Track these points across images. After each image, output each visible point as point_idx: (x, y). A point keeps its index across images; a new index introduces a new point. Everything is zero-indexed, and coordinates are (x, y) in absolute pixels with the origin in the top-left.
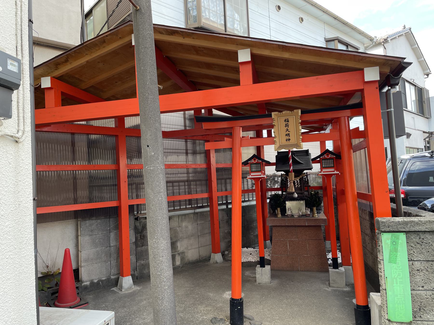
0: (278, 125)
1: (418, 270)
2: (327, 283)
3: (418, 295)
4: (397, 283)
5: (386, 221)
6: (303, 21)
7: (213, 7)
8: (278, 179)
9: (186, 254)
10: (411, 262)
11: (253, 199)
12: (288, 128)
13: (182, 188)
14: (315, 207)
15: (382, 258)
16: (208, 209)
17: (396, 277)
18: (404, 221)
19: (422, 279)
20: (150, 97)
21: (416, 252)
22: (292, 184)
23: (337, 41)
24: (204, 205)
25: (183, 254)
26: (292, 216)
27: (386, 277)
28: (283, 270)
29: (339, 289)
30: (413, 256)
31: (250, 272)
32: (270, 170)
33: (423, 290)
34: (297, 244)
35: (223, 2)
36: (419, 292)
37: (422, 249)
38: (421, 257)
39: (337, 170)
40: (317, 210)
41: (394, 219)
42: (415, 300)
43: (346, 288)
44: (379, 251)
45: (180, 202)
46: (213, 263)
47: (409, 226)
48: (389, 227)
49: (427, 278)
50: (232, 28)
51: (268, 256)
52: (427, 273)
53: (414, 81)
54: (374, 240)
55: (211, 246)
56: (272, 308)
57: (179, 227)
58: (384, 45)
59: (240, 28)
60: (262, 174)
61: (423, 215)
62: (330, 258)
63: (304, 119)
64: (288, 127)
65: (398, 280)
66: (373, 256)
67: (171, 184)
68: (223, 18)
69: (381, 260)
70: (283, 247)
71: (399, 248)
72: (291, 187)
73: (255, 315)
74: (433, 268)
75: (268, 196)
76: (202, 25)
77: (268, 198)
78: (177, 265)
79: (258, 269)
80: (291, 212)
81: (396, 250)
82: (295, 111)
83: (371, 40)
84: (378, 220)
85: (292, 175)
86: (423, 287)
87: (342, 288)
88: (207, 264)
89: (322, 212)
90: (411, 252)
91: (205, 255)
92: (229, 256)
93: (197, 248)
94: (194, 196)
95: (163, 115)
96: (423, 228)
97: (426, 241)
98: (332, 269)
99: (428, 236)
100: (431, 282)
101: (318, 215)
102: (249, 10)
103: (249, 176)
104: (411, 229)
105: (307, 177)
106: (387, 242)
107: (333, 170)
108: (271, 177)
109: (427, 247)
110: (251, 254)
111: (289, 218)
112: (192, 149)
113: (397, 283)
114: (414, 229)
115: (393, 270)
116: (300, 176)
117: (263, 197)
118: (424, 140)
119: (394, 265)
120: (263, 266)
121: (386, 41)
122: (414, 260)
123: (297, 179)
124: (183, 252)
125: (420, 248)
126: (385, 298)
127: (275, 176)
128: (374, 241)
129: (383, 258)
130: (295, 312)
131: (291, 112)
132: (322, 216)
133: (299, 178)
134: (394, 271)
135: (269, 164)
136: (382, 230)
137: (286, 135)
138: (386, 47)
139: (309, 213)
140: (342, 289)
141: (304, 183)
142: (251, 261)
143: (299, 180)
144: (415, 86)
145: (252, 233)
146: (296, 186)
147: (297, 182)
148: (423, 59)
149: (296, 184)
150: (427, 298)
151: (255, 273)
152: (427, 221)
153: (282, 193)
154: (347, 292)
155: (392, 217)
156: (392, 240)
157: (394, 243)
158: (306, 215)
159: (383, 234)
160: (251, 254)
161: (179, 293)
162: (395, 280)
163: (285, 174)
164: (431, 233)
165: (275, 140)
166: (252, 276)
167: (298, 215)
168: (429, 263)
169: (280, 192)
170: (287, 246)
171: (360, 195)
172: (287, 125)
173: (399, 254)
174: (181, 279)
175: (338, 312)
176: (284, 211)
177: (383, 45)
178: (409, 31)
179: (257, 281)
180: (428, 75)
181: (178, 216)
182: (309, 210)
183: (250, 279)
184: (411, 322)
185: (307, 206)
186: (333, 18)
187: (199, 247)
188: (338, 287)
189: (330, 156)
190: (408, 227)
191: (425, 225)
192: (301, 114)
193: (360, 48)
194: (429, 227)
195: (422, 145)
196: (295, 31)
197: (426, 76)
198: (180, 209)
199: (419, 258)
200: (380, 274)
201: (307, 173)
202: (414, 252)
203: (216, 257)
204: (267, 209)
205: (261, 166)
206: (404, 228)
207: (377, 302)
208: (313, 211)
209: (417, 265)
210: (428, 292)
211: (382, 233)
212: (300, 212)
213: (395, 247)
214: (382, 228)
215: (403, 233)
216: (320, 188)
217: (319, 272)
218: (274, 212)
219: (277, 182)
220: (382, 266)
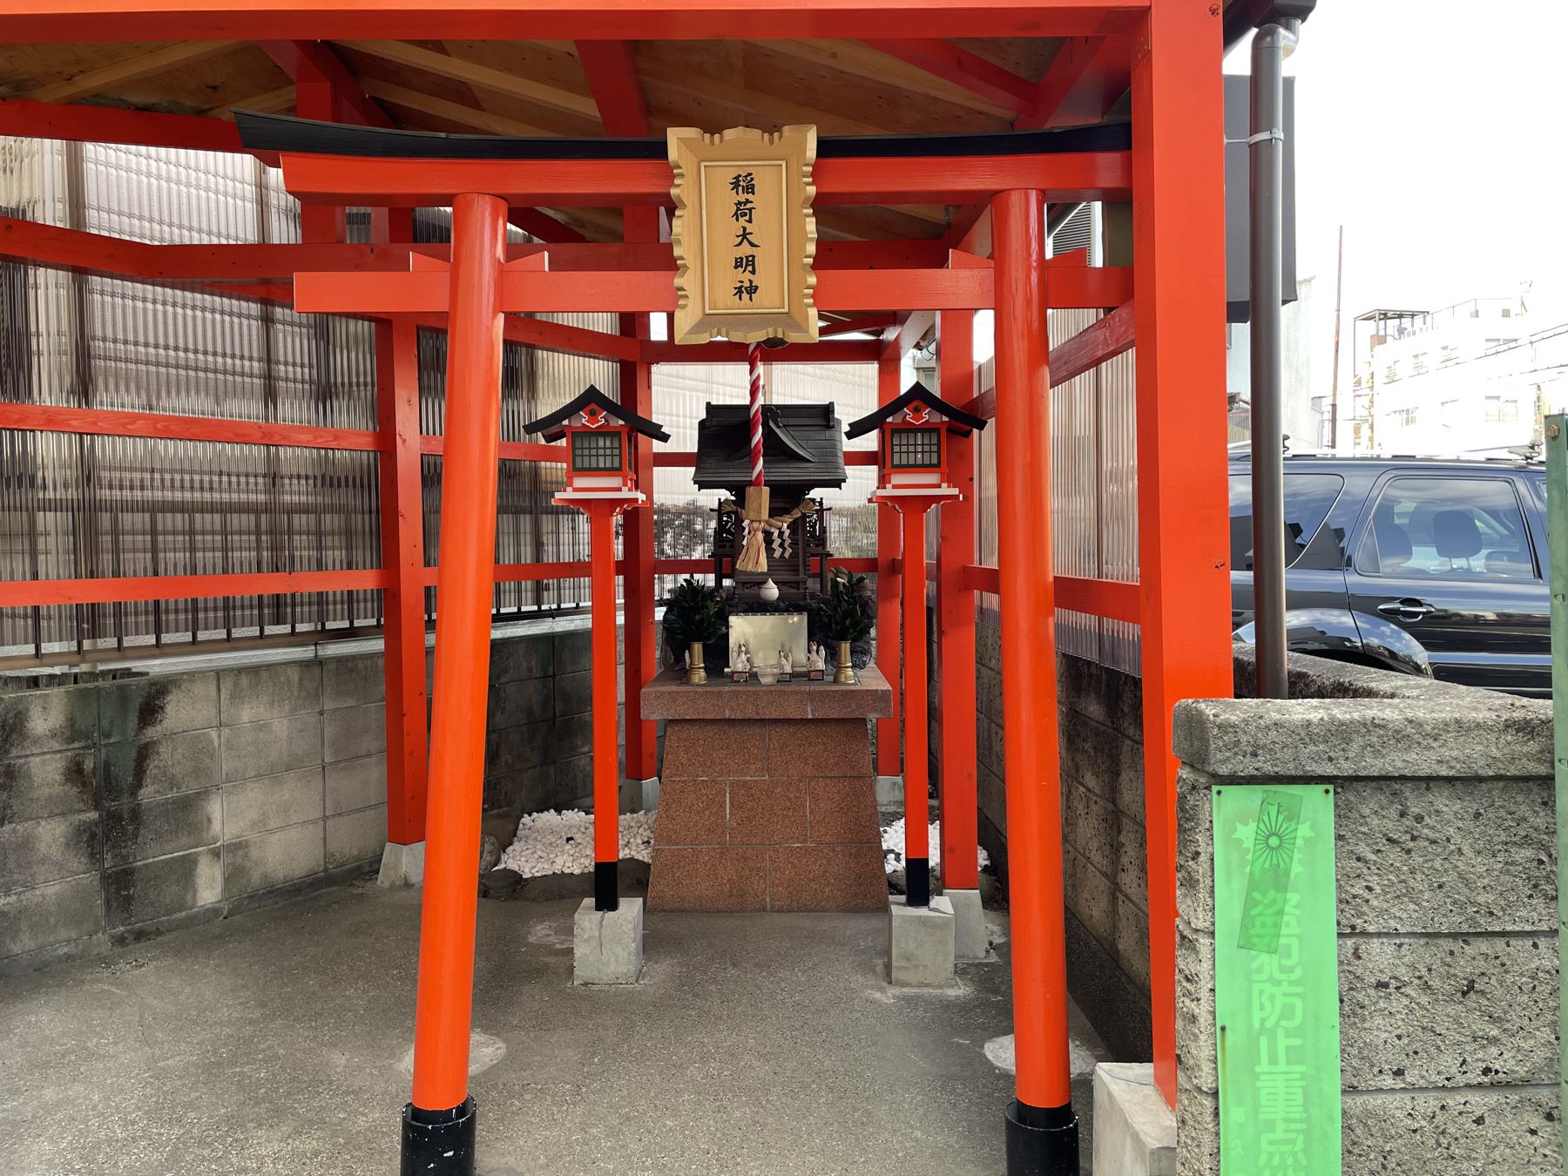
0: (697, 204)
1: (1381, 985)
3: (1369, 1114)
4: (1273, 1060)
5: (1244, 720)
8: (705, 526)
9: (254, 853)
10: (1350, 942)
12: (747, 225)
13: (236, 545)
14: (845, 639)
15: (1207, 924)
16: (378, 645)
17: (1268, 1025)
18: (1333, 720)
19: (1399, 1032)
21: (1378, 889)
22: (760, 536)
24: (357, 623)
25: (241, 853)
26: (753, 676)
27: (1223, 1029)
28: (702, 911)
29: (925, 991)
30: (1365, 908)
31: (554, 925)
33: (1397, 1087)
37: (1413, 872)
39: (952, 483)
40: (852, 652)
41: (1279, 711)
42: (1355, 1143)
43: (957, 985)
44: (1191, 883)
45: (195, 610)
46: (392, 885)
47: (1354, 749)
48: (1256, 755)
49: (1423, 1028)
51: (643, 847)
52: (1424, 1000)
54: (1082, 785)
55: (385, 809)
56: (628, 1119)
60: (625, 484)
61: (1385, 687)
62: (892, 847)
63: (827, 189)
64: (750, 221)
65: (1282, 1042)
66: (1071, 849)
69: (1197, 931)
70: (707, 812)
71: (1296, 868)
72: (755, 549)
73: (541, 1167)
74: (1452, 971)
75: (661, 594)
77: (662, 603)
78: (200, 903)
79: (587, 917)
80: (748, 660)
81: (1279, 880)
84: (1200, 713)
85: (760, 497)
86: (1399, 1073)
87: (941, 987)
88: (360, 891)
89: (872, 664)
90: (1353, 891)
91: (355, 852)
93: (315, 822)
94: (306, 583)
95: (228, 237)
96: (1421, 762)
97: (1433, 828)
98: (904, 905)
99: (1444, 803)
100: (1438, 1048)
101: (855, 675)
103: (565, 491)
104: (1365, 768)
105: (821, 518)
106: (1236, 835)
107: (933, 478)
108: (679, 515)
109: (1437, 864)
110: (571, 839)
111: (740, 689)
112: (306, 361)
113: (1273, 1060)
114: (1379, 763)
115: (1256, 988)
116: (796, 510)
117: (638, 601)
119: (1264, 957)
120: (607, 902)
122: (1364, 934)
123: (780, 524)
124: (240, 843)
125: (1398, 869)
126: (1207, 1139)
127: (693, 511)
128: (1081, 788)
129: (1213, 924)
130: (737, 1133)
131: (766, 136)
132: (871, 679)
133: (788, 519)
134: (1261, 992)
136: (1221, 772)
137: (738, 263)
139: (821, 665)
140: (938, 992)
142: (567, 871)
143: (788, 527)
145: (586, 749)
146: (777, 554)
147: (781, 534)
149: (775, 545)
150: (1415, 1131)
151: (570, 932)
152: (1446, 725)
153: (719, 581)
154: (962, 1007)
155: (1237, 696)
156: (1262, 826)
157: (1274, 841)
158: (807, 676)
159: (1219, 793)
160: (571, 839)
161: (170, 1062)
162: (1263, 1041)
163: (733, 498)
164: (1458, 785)
166: (558, 946)
167: (774, 675)
168: (1436, 945)
169: (709, 580)
170: (722, 806)
171: (1071, 593)
172: (743, 211)
173: (1293, 897)
174: (206, 976)
175: (925, 1114)
176: (718, 654)
179: (577, 972)
181: (218, 673)
182: (823, 652)
183: (547, 965)
187: (325, 818)
188: (922, 985)
189: (927, 415)
190: (1351, 755)
191: (1435, 744)
194: (1455, 753)
198: (230, 643)
199: (1393, 923)
200: (1184, 1004)
202: (1370, 889)
203: (404, 859)
204: (655, 652)
205: (620, 448)
206: (1330, 759)
207: (1137, 1127)
208: (840, 658)
209: (1380, 957)
210: (1420, 1098)
211: (1215, 788)
213: (1275, 861)
214: (1219, 756)
215: (1321, 788)
216: (871, 565)
217: (849, 911)
218: (679, 659)
219: (700, 537)
220: (1206, 965)
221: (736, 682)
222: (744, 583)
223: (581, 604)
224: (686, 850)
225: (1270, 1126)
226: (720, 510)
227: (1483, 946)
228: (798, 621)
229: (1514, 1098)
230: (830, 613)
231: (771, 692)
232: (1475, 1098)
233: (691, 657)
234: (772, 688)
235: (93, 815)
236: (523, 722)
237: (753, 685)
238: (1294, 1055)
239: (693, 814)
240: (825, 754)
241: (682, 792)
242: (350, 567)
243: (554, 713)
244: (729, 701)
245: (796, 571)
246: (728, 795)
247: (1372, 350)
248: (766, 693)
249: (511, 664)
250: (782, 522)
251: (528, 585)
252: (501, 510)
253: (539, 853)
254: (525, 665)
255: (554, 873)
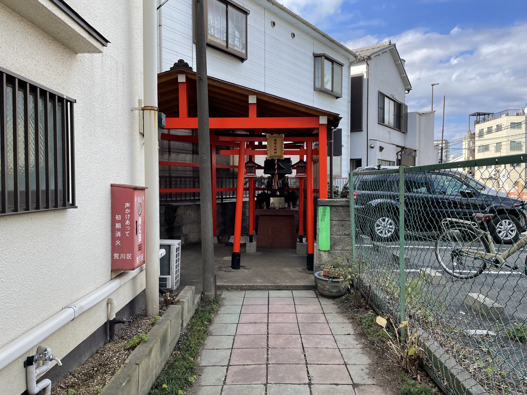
2: (295, 253)
4: (324, 231)
6: (294, 37)
7: (218, 25)
20: (206, 127)
22: (276, 183)
23: (324, 57)
32: (260, 173)
35: (226, 20)
36: (334, 236)
38: (336, 219)
40: (293, 205)
50: (232, 44)
53: (394, 97)
57: (184, 214)
58: (368, 62)
59: (240, 45)
67: (352, 161)
68: (225, 35)
71: (326, 214)
76: (208, 42)
81: (325, 215)
82: (281, 135)
83: (355, 57)
92: (224, 239)
96: (338, 204)
99: (340, 208)
102: (248, 26)
113: (324, 231)
118: (397, 154)
121: (369, 58)
127: (262, 178)
135: (259, 167)
137: (275, 149)
138: (368, 63)
139: (287, 206)
141: (285, 184)
144: (395, 101)
146: (279, 187)
147: (280, 183)
148: (405, 75)
165: (267, 152)
172: (275, 143)
173: (326, 217)
177: (366, 62)
178: (394, 47)
180: (409, 91)
184: (329, 250)
185: (286, 201)
186: (322, 36)
192: (285, 137)
193: (344, 64)
195: (394, 159)
196: (287, 46)
197: (407, 92)
201: (288, 177)
225: (323, 237)
226: (268, 178)
227: (344, 222)
229: (347, 236)
232: (344, 236)
233: (263, 204)
235: (168, 227)
238: (326, 231)
242: (186, 188)
247: (475, 126)
251: (231, 192)
252: (216, 178)
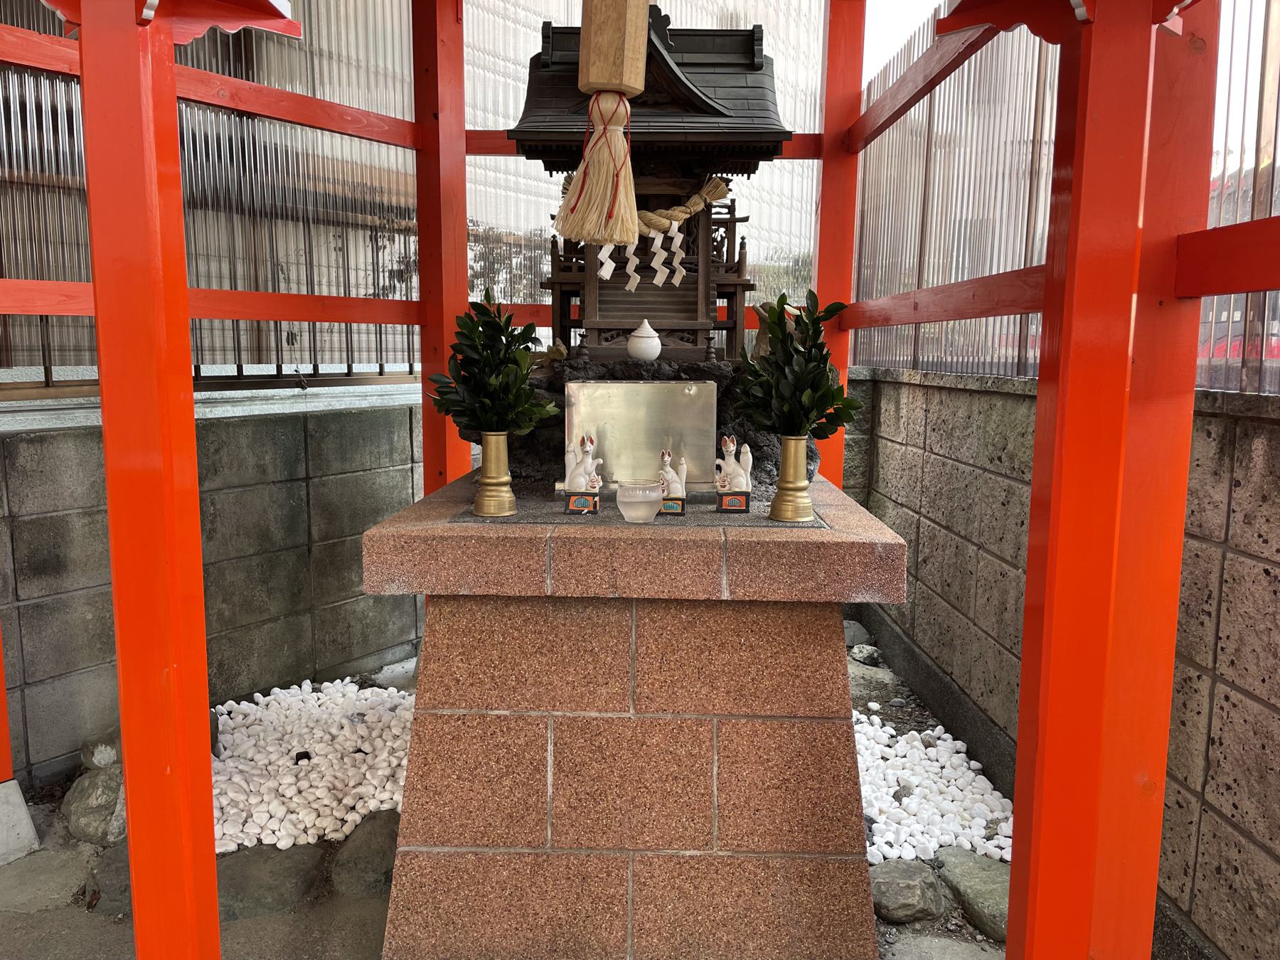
11: (381, 373)
34: (627, 755)
123: (666, 222)
143: (680, 230)
146: (659, 280)
147: (668, 241)
149: (656, 263)
167: (651, 503)
170: (539, 768)
212: (670, 474)
221: (573, 513)
222: (600, 331)
223: (356, 368)
224: (463, 855)
228: (701, 394)
230: (766, 377)
231: (643, 542)
234: (647, 533)
236: (251, 551)
237: (605, 521)
239: (477, 786)
240: (753, 669)
241: (457, 738)
243: (310, 534)
244: (552, 558)
245: (691, 310)
246: (550, 747)
248: (631, 544)
249: (225, 459)
250: (670, 218)
253: (231, 794)
254: (251, 461)
255: (241, 847)
